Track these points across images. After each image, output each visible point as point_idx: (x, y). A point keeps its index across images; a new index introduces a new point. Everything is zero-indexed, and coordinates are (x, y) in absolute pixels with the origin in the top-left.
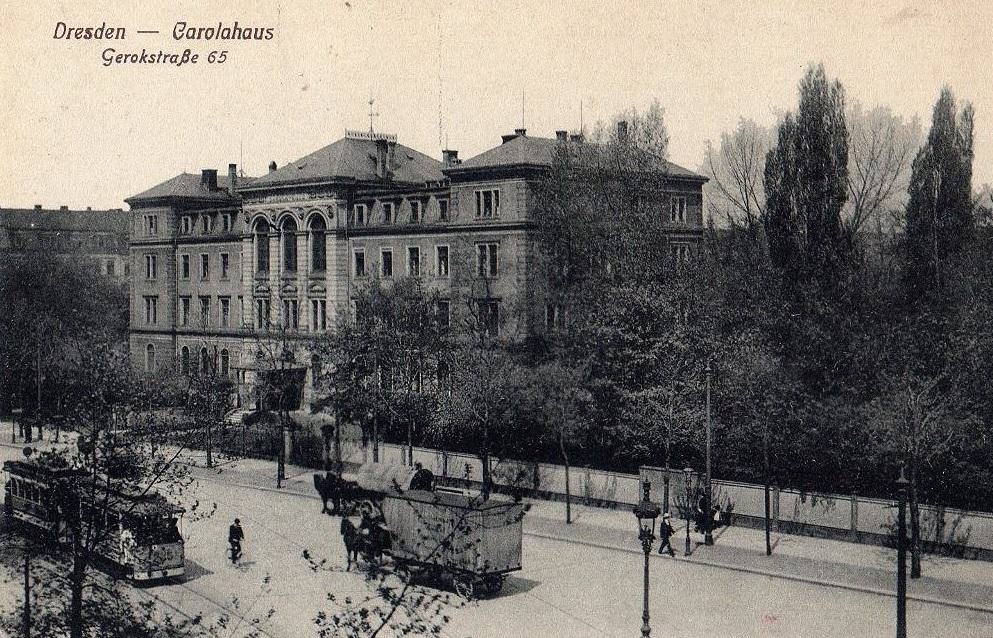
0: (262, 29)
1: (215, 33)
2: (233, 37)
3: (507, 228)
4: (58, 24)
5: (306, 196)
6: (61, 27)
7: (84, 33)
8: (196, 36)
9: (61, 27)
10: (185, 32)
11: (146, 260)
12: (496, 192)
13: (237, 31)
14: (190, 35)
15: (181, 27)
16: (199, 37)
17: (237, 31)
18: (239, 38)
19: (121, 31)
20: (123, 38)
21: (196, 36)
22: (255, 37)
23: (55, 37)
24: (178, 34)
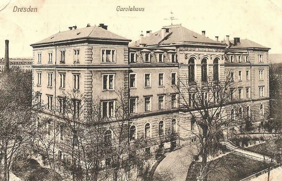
0: (141, 8)
1: (128, 9)
2: (133, 11)
3: (265, 66)
4: (15, 7)
5: (214, 50)
6: (16, 7)
7: (23, 10)
8: (123, 10)
9: (16, 7)
10: (120, 9)
11: (114, 60)
12: (40, 74)
13: (134, 9)
14: (121, 10)
15: (119, 7)
16: (133, 11)
17: (134, 9)
18: (135, 11)
19: (36, 9)
20: (36, 11)
21: (123, 10)
22: (139, 10)
23: (14, 11)
24: (118, 10)
